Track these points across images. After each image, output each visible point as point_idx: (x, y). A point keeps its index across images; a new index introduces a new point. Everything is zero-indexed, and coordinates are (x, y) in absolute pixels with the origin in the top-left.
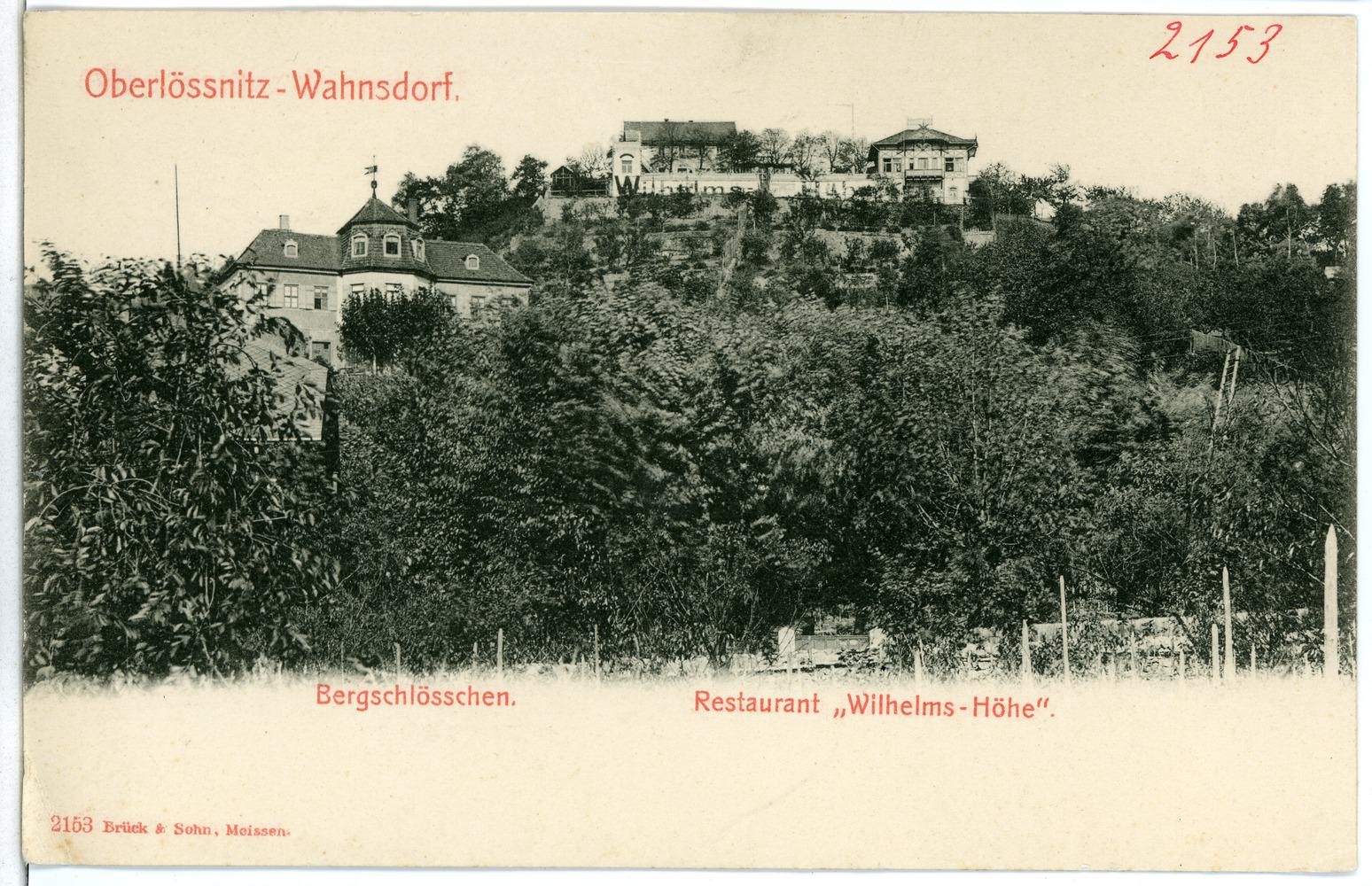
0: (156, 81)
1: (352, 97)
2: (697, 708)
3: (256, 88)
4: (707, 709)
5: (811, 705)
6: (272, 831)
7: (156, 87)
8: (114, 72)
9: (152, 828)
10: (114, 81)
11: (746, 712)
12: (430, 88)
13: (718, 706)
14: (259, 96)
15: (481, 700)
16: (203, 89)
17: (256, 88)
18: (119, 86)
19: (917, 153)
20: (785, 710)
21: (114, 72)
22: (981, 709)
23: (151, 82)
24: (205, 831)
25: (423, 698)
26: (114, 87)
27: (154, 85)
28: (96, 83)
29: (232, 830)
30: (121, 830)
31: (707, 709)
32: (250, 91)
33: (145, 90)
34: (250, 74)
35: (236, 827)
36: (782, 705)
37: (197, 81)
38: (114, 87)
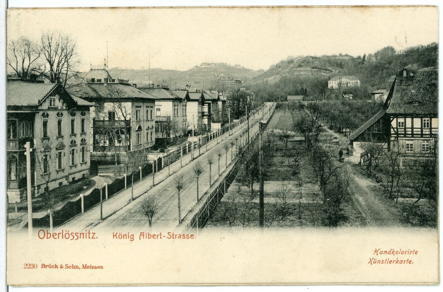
0: (61, 233)
1: (83, 238)
3: (91, 235)
4: (117, 238)
6: (99, 267)
7: (61, 236)
9: (59, 266)
12: (123, 236)
14: (92, 238)
16: (186, 237)
17: (91, 235)
18: (150, 236)
23: (157, 235)
24: (77, 267)
25: (120, 237)
26: (47, 236)
32: (47, 237)
33: (156, 237)
37: (187, 238)
38: (47, 236)
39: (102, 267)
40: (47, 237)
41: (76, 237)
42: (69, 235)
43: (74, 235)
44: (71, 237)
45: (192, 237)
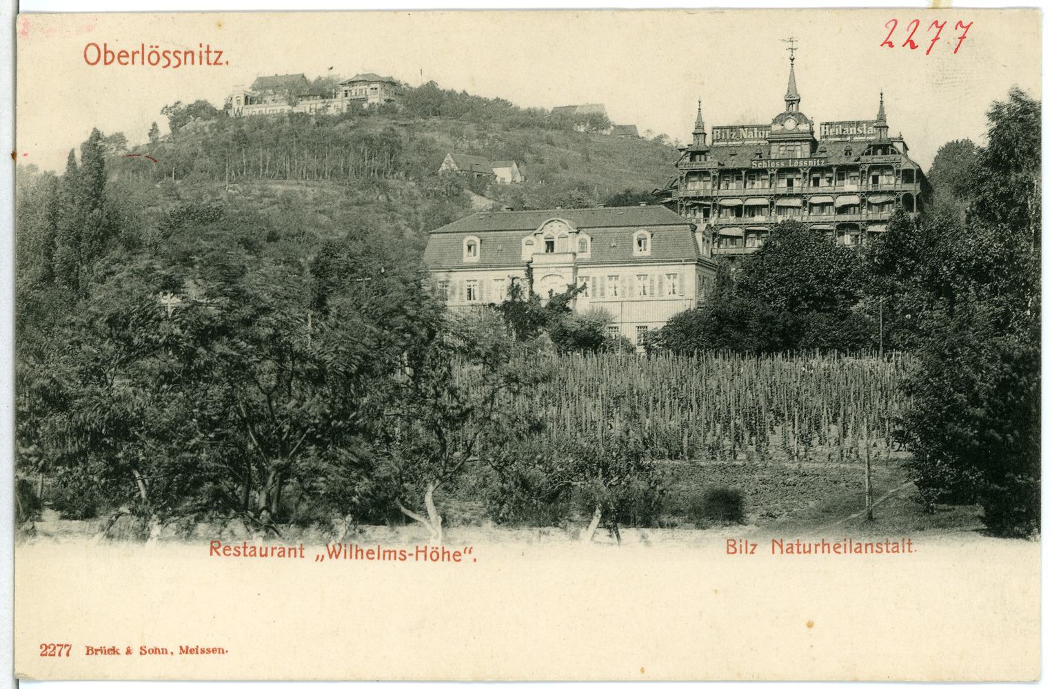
0: (138, 52)
2: (211, 554)
3: (213, 57)
4: (218, 554)
5: (298, 552)
6: (214, 650)
7: (138, 58)
8: (105, 45)
9: (123, 651)
10: (106, 52)
11: (249, 557)
13: (227, 552)
14: (215, 63)
15: (832, 549)
17: (213, 57)
18: (109, 57)
19: (358, 87)
20: (279, 555)
21: (105, 45)
22: (421, 555)
23: (134, 53)
24: (164, 651)
26: (105, 57)
27: (136, 55)
28: (92, 54)
29: (185, 651)
30: (99, 653)
31: (218, 554)
33: (129, 60)
34: (208, 46)
35: (187, 647)
36: (276, 552)
38: (105, 57)
39: (222, 651)
40: (105, 59)
41: (174, 62)
42: (158, 56)
43: (171, 56)
44: (164, 62)
45: (123, 60)
